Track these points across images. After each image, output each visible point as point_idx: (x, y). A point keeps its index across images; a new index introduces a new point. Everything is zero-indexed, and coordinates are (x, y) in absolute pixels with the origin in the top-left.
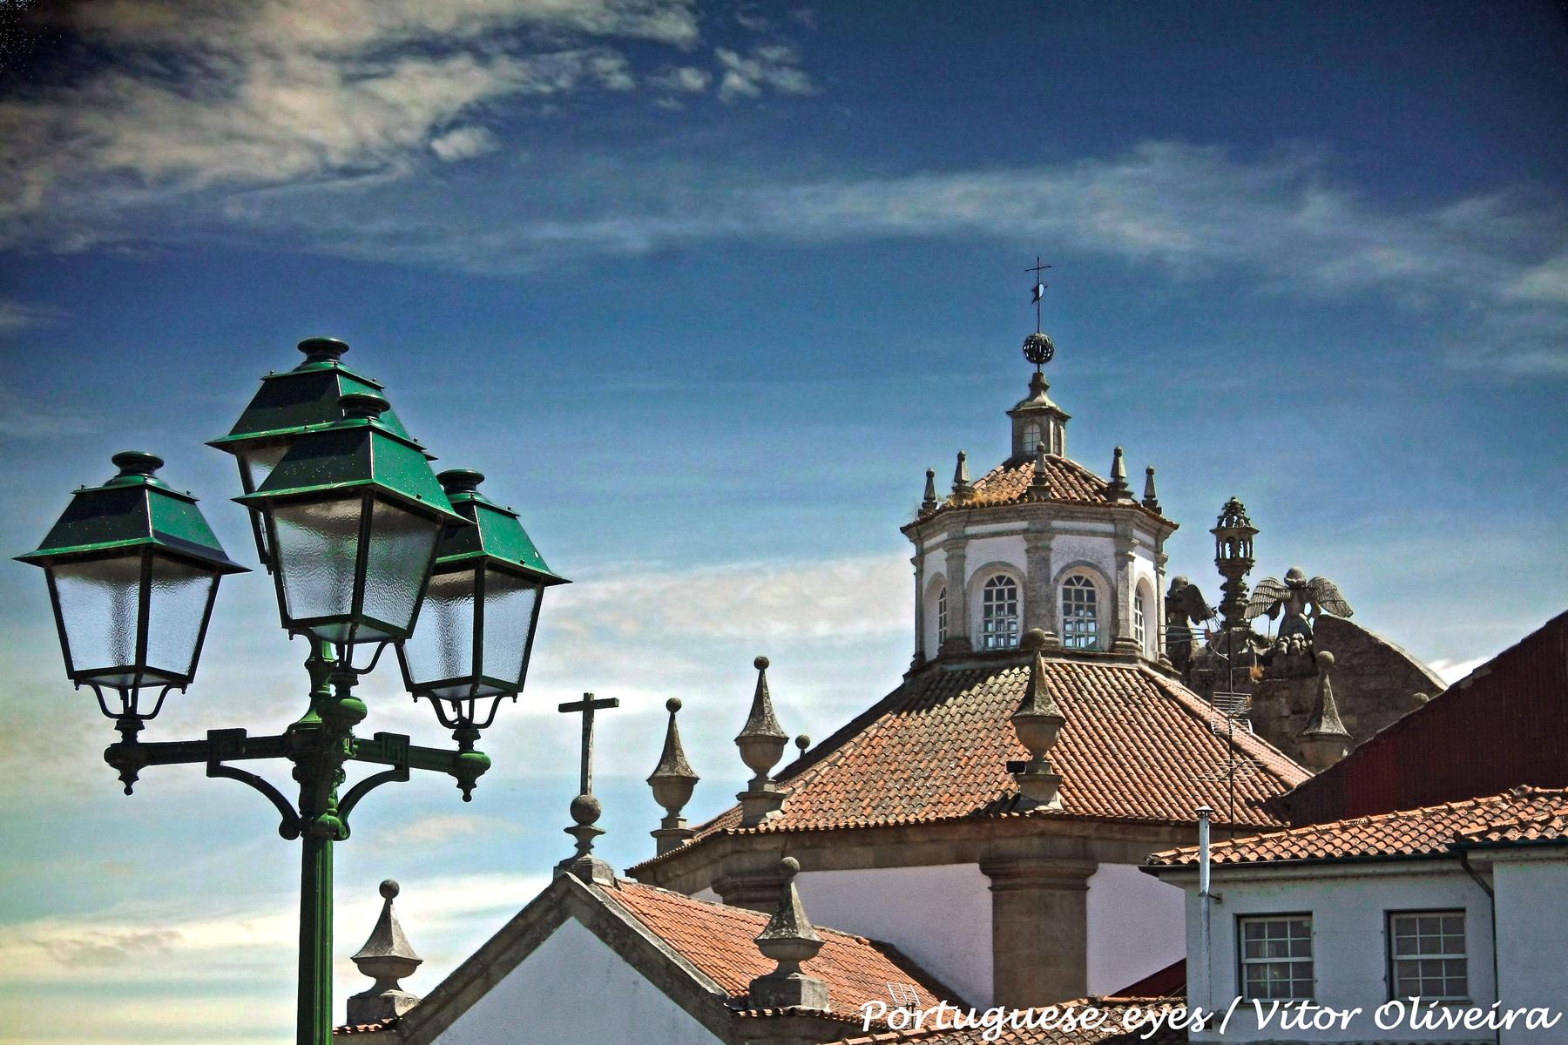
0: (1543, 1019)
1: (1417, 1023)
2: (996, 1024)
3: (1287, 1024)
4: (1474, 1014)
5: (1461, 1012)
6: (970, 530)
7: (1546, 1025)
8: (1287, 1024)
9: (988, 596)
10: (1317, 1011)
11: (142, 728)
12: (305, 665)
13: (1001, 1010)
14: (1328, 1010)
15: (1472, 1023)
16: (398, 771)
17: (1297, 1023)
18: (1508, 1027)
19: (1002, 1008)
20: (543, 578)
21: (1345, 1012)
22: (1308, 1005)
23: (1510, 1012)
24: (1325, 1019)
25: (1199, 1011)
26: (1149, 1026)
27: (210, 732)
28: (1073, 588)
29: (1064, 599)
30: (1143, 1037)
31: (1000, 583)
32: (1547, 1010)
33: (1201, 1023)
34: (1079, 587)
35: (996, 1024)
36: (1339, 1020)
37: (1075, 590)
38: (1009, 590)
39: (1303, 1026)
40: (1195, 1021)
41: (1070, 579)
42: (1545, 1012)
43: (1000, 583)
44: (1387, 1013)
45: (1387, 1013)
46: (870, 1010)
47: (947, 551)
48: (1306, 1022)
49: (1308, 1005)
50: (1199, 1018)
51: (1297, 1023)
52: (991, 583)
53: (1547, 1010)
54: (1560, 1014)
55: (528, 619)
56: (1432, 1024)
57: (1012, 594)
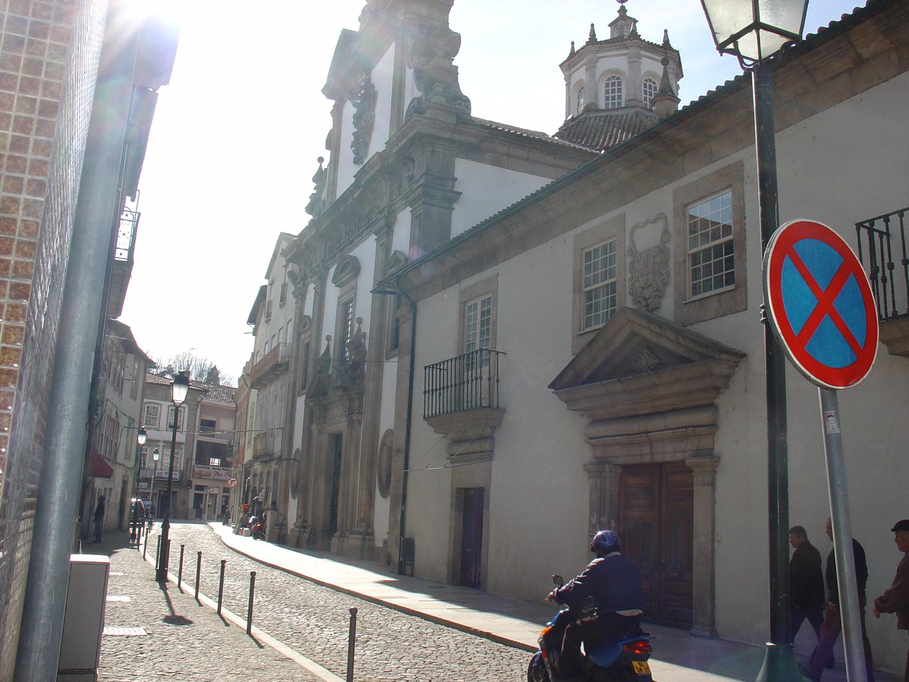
6: (599, 55)
9: (607, 85)
11: (589, 39)
12: (855, 9)
16: (256, 322)
20: (469, 112)
28: (610, 82)
31: (613, 79)
37: (611, 83)
38: (618, 82)
41: (609, 78)
43: (613, 79)
47: (628, 58)
52: (609, 79)
55: (706, 21)
57: (620, 84)
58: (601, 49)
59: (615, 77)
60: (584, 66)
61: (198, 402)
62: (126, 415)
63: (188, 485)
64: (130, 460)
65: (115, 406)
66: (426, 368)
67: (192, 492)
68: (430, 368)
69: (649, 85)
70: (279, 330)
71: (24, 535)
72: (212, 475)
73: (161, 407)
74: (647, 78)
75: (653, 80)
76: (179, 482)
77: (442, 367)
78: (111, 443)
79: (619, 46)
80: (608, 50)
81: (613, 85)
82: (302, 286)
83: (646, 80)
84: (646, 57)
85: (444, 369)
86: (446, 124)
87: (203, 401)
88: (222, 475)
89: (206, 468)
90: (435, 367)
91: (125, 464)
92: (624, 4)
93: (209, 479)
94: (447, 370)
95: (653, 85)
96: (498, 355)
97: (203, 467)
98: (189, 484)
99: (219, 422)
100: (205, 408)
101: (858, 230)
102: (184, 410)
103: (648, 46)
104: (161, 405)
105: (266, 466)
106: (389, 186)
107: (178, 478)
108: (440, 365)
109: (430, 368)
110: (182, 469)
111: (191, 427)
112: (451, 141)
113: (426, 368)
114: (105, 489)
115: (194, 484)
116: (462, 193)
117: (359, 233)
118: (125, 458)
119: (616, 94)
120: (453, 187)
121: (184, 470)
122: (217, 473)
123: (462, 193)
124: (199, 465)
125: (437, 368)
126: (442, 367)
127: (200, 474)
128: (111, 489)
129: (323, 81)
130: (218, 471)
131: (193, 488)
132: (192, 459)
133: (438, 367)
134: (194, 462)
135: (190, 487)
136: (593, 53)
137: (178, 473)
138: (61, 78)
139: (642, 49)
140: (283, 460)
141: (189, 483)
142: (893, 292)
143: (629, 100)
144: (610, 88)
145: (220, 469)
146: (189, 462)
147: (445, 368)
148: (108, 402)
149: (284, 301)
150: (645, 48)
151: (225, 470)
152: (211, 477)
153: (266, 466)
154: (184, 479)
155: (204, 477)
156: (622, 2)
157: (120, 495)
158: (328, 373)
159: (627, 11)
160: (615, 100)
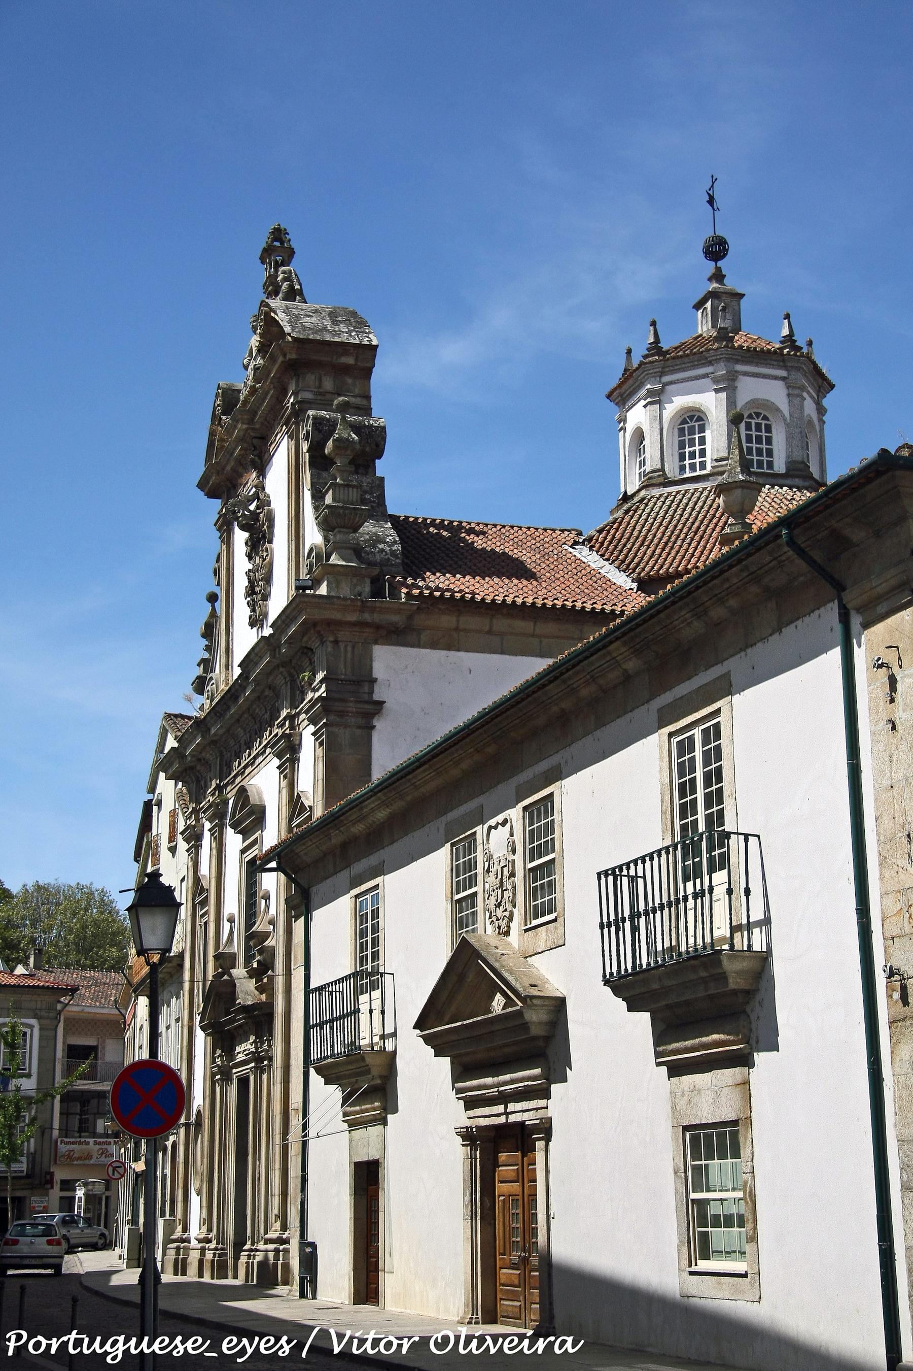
0: (569, 1345)
1: (465, 1349)
2: (117, 1349)
3: (358, 1349)
4: (268, 1341)
5: (257, 1339)
6: (666, 379)
7: (571, 1351)
8: (358, 1349)
10: (382, 1339)
13: (121, 1338)
14: (40, 1338)
15: (510, 1349)
17: (366, 1349)
18: (540, 1352)
19: (123, 1337)
21: (55, 1340)
22: (77, 1334)
23: (541, 1340)
24: (37, 1345)
25: (285, 1338)
26: (243, 1351)
27: (382, 479)
28: (686, 426)
29: (772, 449)
30: (239, 1360)
31: (691, 421)
32: (571, 1338)
33: (287, 1348)
34: (759, 421)
35: (117, 1349)
36: (49, 1346)
37: (688, 427)
38: (699, 425)
39: (370, 1352)
40: (282, 1347)
42: (570, 1340)
44: (439, 1341)
45: (439, 1341)
46: (14, 1338)
48: (373, 1349)
49: (77, 1334)
50: (285, 1345)
51: (366, 1349)
53: (571, 1338)
54: (582, 1342)
56: (477, 1349)
58: (667, 369)
59: (694, 416)
60: (642, 401)
61: (60, 1013)
63: (47, 1182)
66: (599, 874)
68: (607, 875)
69: (756, 424)
72: (94, 1157)
74: (752, 411)
75: (764, 413)
76: (28, 1176)
77: (632, 873)
81: (692, 432)
82: (193, 823)
83: (750, 416)
84: (746, 374)
85: (339, 992)
86: (349, 602)
87: (68, 1008)
89: (80, 1143)
90: (618, 873)
92: (720, 264)
93: (88, 1165)
94: (644, 877)
95: (763, 422)
96: (746, 841)
97: (73, 1143)
98: (48, 1181)
99: (104, 1048)
100: (75, 1024)
101: (599, 879)
102: (32, 1031)
103: (749, 354)
106: (289, 683)
107: (25, 1169)
108: (628, 868)
109: (668, 853)
110: (32, 1150)
111: (46, 1061)
112: (362, 624)
113: (599, 874)
116: (384, 702)
117: (240, 768)
119: (697, 448)
120: (371, 692)
121: (35, 1151)
123: (384, 702)
124: (66, 1140)
125: (621, 876)
126: (632, 873)
127: (69, 1157)
129: (199, 469)
130: (105, 1146)
131: (57, 1187)
132: (52, 1128)
133: (625, 872)
134: (56, 1133)
135: (49, 1186)
136: (655, 377)
137: (24, 1159)
139: (737, 361)
141: (48, 1177)
142: (603, 951)
143: (717, 460)
144: (687, 438)
146: (46, 1136)
147: (640, 873)
149: (174, 841)
150: (744, 359)
152: (92, 1162)
155: (79, 1162)
156: (716, 261)
159: (725, 276)
160: (700, 450)
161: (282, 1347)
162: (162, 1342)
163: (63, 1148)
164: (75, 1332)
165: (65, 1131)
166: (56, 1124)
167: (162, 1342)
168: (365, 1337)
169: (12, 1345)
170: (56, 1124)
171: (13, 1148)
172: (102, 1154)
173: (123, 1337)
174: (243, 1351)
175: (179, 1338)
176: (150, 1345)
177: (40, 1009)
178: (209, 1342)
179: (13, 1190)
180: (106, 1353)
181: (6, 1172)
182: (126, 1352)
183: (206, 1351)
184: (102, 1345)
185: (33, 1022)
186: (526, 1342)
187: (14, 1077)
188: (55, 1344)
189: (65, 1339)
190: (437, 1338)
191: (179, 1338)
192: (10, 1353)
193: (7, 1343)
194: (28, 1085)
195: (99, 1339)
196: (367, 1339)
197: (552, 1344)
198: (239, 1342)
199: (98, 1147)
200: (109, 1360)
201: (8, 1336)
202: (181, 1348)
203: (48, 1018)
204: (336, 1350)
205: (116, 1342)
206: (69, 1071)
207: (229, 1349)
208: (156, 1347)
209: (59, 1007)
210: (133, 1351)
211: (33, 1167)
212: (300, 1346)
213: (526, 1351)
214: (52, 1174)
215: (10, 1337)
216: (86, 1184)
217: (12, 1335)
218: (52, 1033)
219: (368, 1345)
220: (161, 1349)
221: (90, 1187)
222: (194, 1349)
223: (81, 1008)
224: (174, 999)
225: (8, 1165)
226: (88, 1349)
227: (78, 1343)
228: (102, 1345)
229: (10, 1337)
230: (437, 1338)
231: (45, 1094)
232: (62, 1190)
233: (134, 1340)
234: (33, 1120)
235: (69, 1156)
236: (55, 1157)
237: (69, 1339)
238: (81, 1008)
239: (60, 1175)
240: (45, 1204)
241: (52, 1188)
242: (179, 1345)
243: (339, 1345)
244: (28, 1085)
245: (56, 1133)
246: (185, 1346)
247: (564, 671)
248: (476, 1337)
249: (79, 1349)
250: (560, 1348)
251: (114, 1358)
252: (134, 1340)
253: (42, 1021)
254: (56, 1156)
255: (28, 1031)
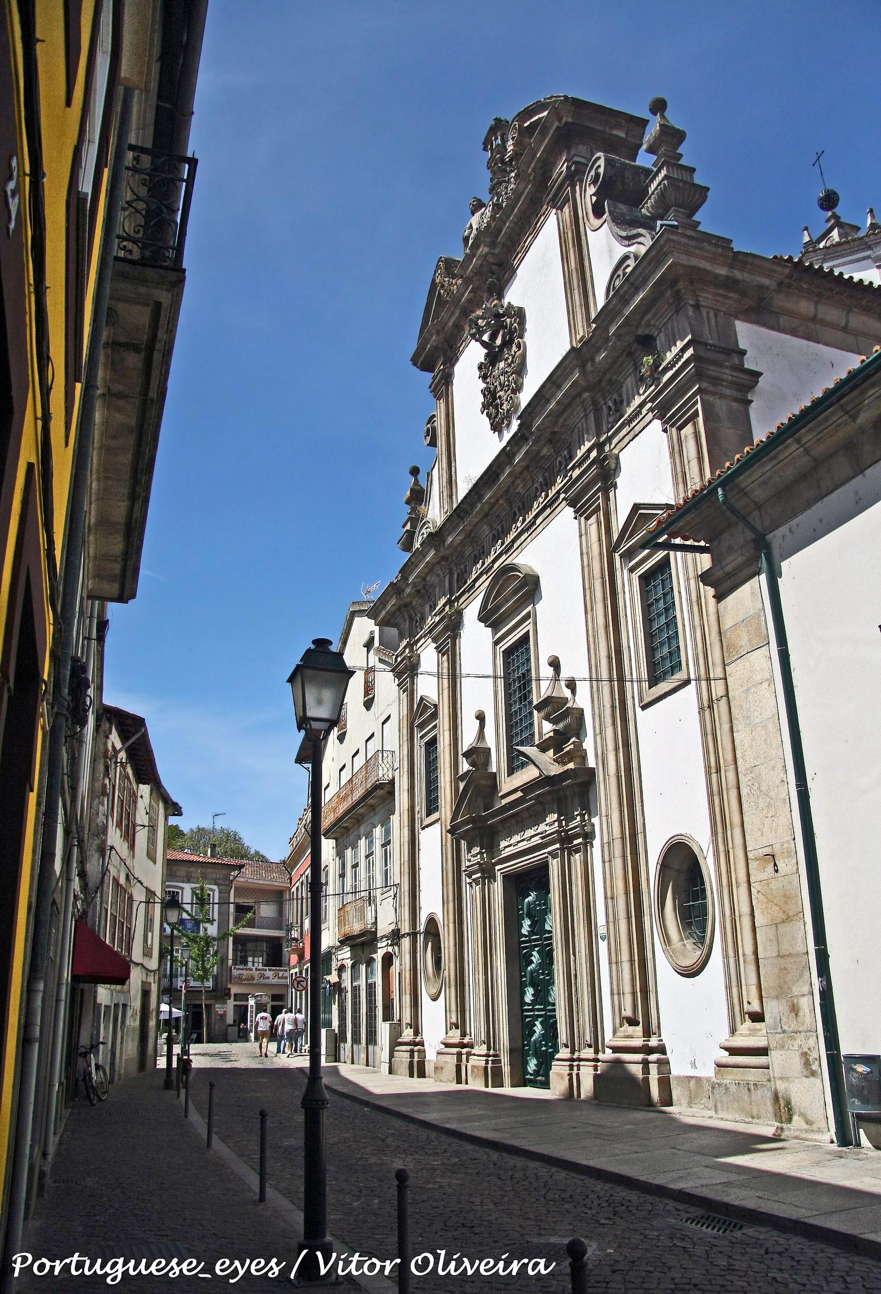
0: (541, 1267)
1: (443, 1270)
2: (117, 1271)
3: (343, 1271)
7: (543, 1272)
8: (343, 1271)
14: (44, 1260)
19: (122, 1259)
23: (516, 1262)
24: (42, 1267)
26: (235, 1272)
30: (231, 1281)
33: (276, 1270)
35: (117, 1271)
36: (52, 1268)
40: (271, 1268)
42: (542, 1261)
44: (420, 1263)
45: (420, 1263)
46: (19, 1260)
48: (357, 1270)
50: (274, 1266)
61: (232, 882)
62: (142, 884)
64: (151, 957)
65: (125, 864)
67: (231, 1003)
70: (367, 741)
71: (446, 827)
72: (256, 979)
73: (182, 892)
76: (213, 991)
78: (120, 927)
79: (857, 247)
80: (839, 256)
87: (237, 879)
88: (268, 978)
91: (145, 964)
97: (242, 969)
98: (227, 994)
104: (182, 889)
105: (363, 953)
111: (224, 915)
114: (116, 1005)
115: (232, 993)
118: (144, 955)
121: (218, 973)
122: (262, 976)
128: (125, 1006)
131: (232, 998)
134: (230, 962)
135: (227, 998)
138: (112, 991)
140: (403, 936)
145: (266, 970)
146: (224, 965)
148: (113, 852)
151: (273, 970)
152: (255, 982)
153: (363, 953)
154: (219, 986)
155: (246, 982)
157: (138, 1013)
158: (487, 770)
161: (271, 1268)
162: (158, 1264)
163: (235, 973)
164: (77, 1254)
165: (235, 962)
166: (230, 956)
167: (158, 1264)
168: (350, 1259)
169: (18, 1266)
170: (230, 956)
171: (205, 970)
172: (261, 977)
173: (122, 1259)
174: (235, 1272)
175: (175, 1260)
176: (147, 1267)
177: (219, 879)
178: (203, 1263)
179: (206, 999)
180: (107, 1275)
181: (200, 987)
182: (125, 1273)
183: (200, 1272)
184: (102, 1268)
185: (215, 887)
186: (501, 1264)
187: (203, 922)
188: (58, 1266)
189: (68, 1261)
190: (417, 1261)
191: (175, 1260)
192: (16, 1274)
193: (13, 1265)
194: (213, 930)
195: (99, 1261)
196: (352, 1261)
197: (525, 1266)
198: (232, 1264)
199: (258, 972)
200: (109, 1280)
201: (14, 1258)
202: (177, 1270)
203: (224, 885)
204: (323, 1271)
205: (116, 1263)
206: (237, 921)
207: (222, 1270)
208: (153, 1268)
209: (231, 878)
210: (132, 1273)
211: (216, 984)
212: (288, 1268)
213: (501, 1273)
214: (229, 989)
215: (16, 1259)
216: (253, 996)
217: (18, 1257)
218: (226, 895)
219: (353, 1267)
220: (158, 1270)
221: (259, 999)
222: (189, 1270)
223: (246, 879)
224: (350, 850)
225: (203, 982)
226: (89, 1270)
227: (80, 1265)
228: (102, 1268)
229: (16, 1259)
230: (417, 1261)
231: (223, 936)
232: (235, 1000)
233: (133, 1262)
234: (216, 954)
235: (240, 977)
236: (231, 979)
237: (72, 1261)
238: (246, 879)
239: (235, 990)
240: (225, 1009)
241: (230, 999)
242: (175, 1266)
243: (325, 1265)
244: (213, 930)
245: (230, 962)
246: (180, 1268)
247: (40, 799)
248: (454, 1260)
249: (81, 1270)
250: (533, 1270)
251: (113, 1279)
252: (133, 1262)
253: (220, 887)
254: (231, 977)
255: (211, 893)
